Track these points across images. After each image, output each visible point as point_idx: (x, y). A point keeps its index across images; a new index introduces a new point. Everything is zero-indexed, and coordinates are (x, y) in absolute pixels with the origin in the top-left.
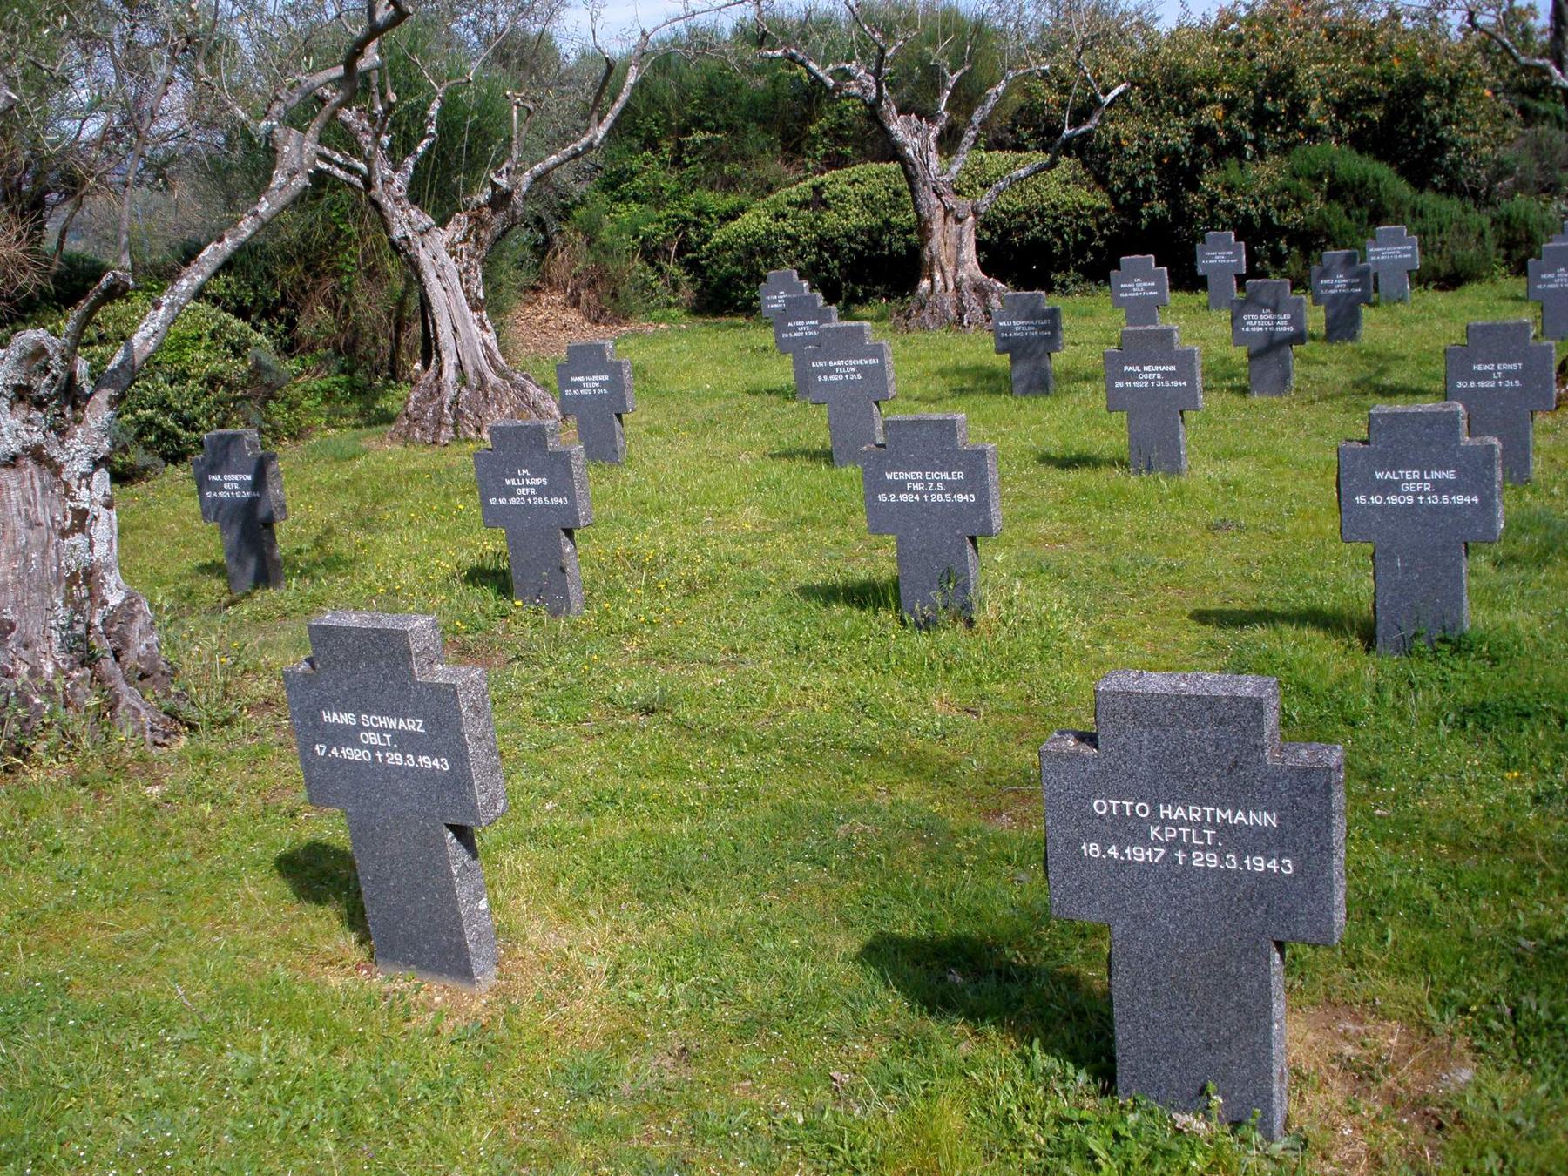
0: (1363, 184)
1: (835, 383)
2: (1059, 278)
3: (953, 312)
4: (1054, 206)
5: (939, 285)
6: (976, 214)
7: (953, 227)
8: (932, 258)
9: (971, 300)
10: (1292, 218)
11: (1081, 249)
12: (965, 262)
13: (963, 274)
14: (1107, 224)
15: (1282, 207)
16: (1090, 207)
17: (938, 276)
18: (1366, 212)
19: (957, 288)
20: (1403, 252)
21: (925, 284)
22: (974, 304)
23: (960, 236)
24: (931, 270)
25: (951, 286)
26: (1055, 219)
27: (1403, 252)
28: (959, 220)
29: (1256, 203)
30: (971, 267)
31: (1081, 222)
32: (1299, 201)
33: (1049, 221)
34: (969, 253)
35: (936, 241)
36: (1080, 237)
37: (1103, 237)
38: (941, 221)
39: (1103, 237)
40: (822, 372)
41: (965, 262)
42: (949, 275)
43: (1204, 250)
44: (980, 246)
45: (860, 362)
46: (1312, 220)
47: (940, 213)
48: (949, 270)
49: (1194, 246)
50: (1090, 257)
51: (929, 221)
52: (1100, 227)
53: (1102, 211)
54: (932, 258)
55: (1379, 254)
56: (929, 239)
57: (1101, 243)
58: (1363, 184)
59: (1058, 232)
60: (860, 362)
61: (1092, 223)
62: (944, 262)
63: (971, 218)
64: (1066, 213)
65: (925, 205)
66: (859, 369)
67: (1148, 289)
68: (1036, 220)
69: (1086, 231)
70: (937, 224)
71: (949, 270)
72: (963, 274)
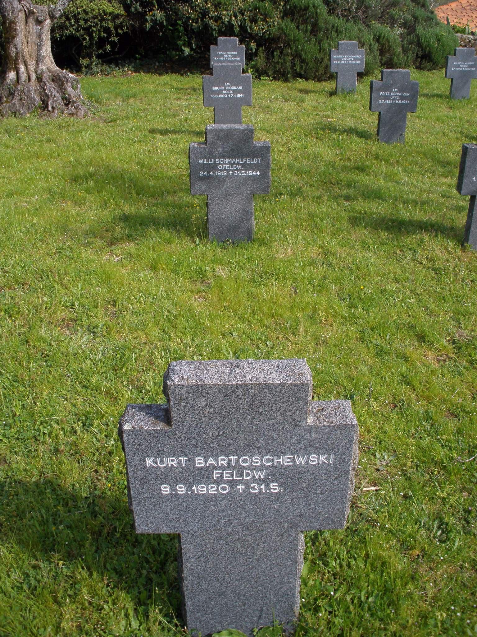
0: (306, 8)
1: (208, 499)
2: (84, 62)
3: (38, 99)
4: (85, 12)
5: (24, 77)
6: (52, 17)
7: (34, 28)
8: (17, 54)
9: (51, 88)
10: (259, 28)
11: (102, 42)
12: (44, 57)
13: (43, 67)
14: (121, 26)
15: (254, 20)
16: (110, 14)
17: (22, 69)
18: (309, 28)
19: (39, 79)
20: (356, 59)
21: (12, 75)
22: (55, 93)
23: (40, 36)
24: (16, 64)
25: (33, 77)
26: (86, 21)
27: (356, 59)
28: (39, 22)
29: (236, 16)
30: (49, 63)
31: (104, 24)
32: (266, 16)
33: (82, 23)
34: (47, 49)
35: (19, 40)
36: (102, 34)
37: (117, 35)
38: (23, 23)
39: (117, 35)
40: (170, 477)
41: (44, 57)
42: (31, 68)
43: (216, 50)
44: (54, 41)
45: (285, 460)
46: (274, 30)
47: (22, 16)
48: (32, 64)
49: (209, 46)
50: (109, 48)
51: (13, 22)
52: (116, 28)
53: (117, 16)
54: (17, 54)
55: (340, 59)
56: (14, 37)
57: (116, 39)
58: (306, 8)
59: (88, 30)
60: (285, 460)
61: (111, 25)
62: (27, 57)
63: (48, 21)
64: (95, 17)
65: (9, 8)
66: (276, 473)
67: (235, 92)
68: (73, 21)
69: (107, 30)
70: (20, 26)
71: (32, 64)
72: (43, 67)
